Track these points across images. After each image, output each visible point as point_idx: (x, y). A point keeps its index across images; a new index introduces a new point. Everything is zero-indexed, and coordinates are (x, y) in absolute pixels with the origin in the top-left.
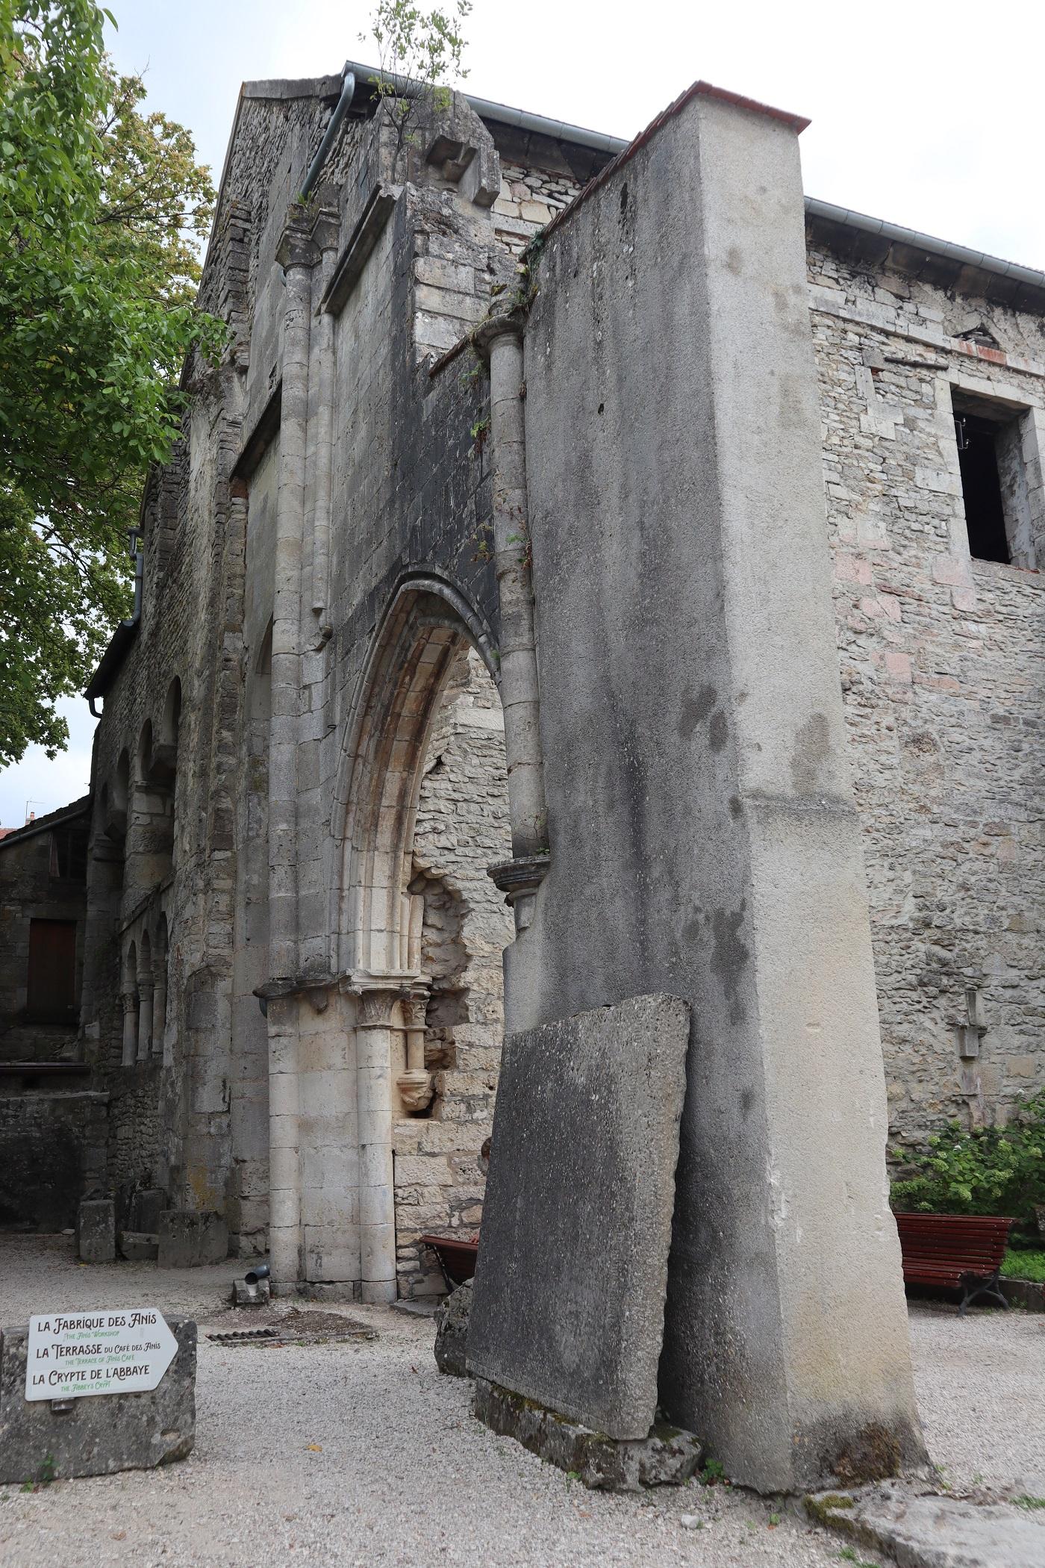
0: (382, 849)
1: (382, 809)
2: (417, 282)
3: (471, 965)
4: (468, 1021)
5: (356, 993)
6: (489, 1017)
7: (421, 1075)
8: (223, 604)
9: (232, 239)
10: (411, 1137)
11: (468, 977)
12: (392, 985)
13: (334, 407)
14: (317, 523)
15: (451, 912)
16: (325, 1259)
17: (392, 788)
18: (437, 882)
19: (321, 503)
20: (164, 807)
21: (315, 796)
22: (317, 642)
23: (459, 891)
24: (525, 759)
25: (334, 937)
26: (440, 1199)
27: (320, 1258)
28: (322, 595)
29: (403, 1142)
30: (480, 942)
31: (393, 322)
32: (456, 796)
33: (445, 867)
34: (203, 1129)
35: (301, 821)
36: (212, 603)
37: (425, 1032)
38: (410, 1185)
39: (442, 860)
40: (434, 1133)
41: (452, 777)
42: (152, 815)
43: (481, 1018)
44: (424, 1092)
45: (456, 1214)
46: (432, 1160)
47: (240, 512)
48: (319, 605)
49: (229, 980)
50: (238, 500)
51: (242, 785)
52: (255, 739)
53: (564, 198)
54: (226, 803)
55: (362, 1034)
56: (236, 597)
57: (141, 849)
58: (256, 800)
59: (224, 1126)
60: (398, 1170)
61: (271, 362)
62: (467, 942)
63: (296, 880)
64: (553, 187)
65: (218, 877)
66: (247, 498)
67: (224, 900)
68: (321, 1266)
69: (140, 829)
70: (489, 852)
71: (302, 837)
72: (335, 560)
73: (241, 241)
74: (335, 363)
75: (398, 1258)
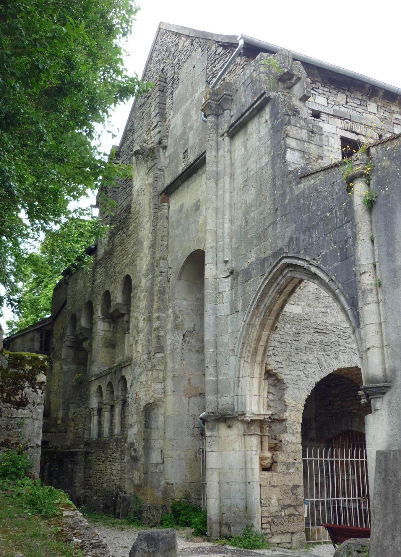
0: (258, 363)
1: (259, 347)
2: (287, 136)
3: (288, 410)
4: (287, 432)
5: (247, 420)
6: (295, 431)
7: (268, 454)
8: (158, 247)
9: (159, 90)
10: (267, 479)
11: (287, 414)
12: (261, 418)
13: (232, 176)
14: (225, 225)
15: (278, 387)
16: (232, 528)
17: (264, 338)
18: (275, 375)
19: (227, 217)
20: (110, 328)
21: (226, 338)
22: (227, 274)
23: (283, 379)
24: (376, 345)
25: (236, 397)
26: (277, 505)
27: (230, 527)
28: (228, 255)
29: (264, 481)
30: (291, 400)
31: (271, 149)
32: (282, 340)
33: (278, 370)
34: (153, 470)
35: (219, 348)
36: (152, 246)
37: (268, 436)
38: (266, 499)
39: (277, 367)
40: (274, 477)
41: (280, 332)
42: (105, 331)
43: (291, 431)
44: (269, 461)
45: (283, 510)
46: (274, 489)
47: (166, 209)
48: (227, 259)
49: (163, 408)
50: (166, 204)
51: (169, 326)
52: (176, 307)
53: (318, 90)
54: (162, 333)
55: (248, 437)
56: (165, 245)
57: (101, 346)
58: (177, 333)
59: (162, 468)
60: (262, 493)
61: (184, 147)
62: (286, 400)
63: (217, 372)
64: (314, 86)
65: (159, 365)
66: (168, 202)
67: (161, 374)
68: (230, 530)
69: (101, 337)
70: (294, 363)
71: (219, 354)
72: (234, 241)
73: (163, 91)
74: (231, 158)
75: (262, 528)
